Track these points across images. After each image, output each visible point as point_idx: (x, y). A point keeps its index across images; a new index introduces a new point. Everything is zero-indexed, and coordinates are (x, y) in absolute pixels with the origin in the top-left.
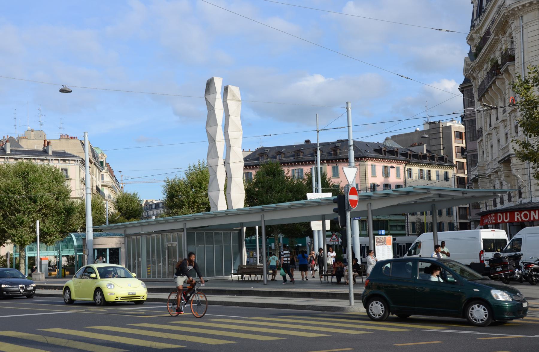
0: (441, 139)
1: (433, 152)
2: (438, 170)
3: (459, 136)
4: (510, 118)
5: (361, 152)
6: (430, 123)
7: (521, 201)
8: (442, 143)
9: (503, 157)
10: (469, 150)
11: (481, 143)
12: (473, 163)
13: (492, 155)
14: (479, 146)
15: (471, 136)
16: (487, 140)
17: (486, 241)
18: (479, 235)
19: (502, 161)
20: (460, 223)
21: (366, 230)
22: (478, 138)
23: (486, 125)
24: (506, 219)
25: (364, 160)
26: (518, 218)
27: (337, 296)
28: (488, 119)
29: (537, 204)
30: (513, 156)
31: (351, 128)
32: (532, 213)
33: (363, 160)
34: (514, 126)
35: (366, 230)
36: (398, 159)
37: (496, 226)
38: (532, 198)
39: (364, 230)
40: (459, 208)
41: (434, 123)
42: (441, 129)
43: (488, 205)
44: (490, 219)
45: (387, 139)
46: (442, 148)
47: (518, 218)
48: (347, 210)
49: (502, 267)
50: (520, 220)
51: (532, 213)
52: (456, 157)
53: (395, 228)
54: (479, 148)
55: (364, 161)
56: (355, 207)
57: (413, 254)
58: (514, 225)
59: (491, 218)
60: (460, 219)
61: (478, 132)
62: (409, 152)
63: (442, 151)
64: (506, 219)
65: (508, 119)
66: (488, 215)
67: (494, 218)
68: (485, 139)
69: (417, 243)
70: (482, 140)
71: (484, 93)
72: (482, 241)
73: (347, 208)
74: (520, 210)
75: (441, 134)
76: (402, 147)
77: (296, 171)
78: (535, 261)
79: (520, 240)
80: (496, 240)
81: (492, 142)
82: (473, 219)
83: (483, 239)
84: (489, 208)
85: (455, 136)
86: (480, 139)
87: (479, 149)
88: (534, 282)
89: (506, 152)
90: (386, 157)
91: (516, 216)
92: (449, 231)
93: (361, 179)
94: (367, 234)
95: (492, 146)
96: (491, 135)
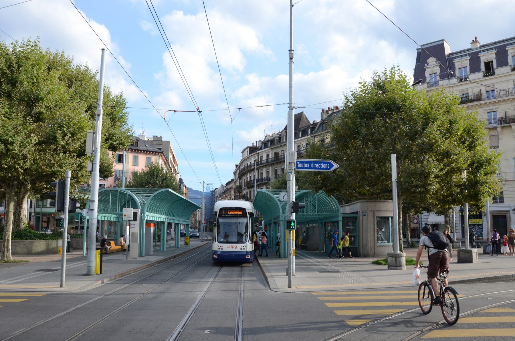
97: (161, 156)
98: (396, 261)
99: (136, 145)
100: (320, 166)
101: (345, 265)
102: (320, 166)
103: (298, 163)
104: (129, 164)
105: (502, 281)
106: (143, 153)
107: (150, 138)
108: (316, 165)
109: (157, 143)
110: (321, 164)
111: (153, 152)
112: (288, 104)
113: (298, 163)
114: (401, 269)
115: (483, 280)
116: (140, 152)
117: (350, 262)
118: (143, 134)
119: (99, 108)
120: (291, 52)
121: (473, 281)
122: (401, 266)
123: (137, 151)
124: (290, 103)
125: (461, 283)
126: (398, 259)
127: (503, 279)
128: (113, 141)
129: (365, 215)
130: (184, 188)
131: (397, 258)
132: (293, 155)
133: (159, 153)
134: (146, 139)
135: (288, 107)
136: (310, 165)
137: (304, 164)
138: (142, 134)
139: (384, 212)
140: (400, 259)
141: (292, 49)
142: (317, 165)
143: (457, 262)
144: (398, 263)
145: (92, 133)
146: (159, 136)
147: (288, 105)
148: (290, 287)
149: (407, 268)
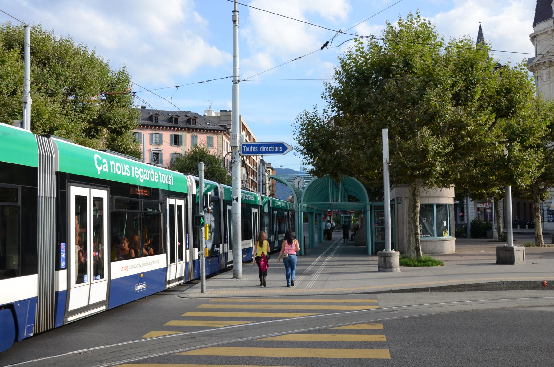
77: (154, 135)
97: (225, 134)
98: (385, 261)
99: (195, 123)
100: (271, 149)
101: (344, 265)
102: (271, 149)
103: (245, 146)
104: (186, 145)
105: (486, 290)
106: (202, 132)
107: (219, 113)
108: (266, 149)
109: (226, 118)
110: (272, 147)
111: (214, 130)
112: (232, 77)
113: (245, 146)
114: (391, 271)
115: (458, 288)
116: (206, 132)
117: (484, 256)
118: (210, 108)
119: (26, 94)
120: (235, 13)
121: (441, 289)
122: (391, 267)
123: (195, 130)
124: (234, 77)
125: (423, 290)
126: (387, 258)
127: (488, 287)
128: (112, 125)
129: (400, 203)
130: (271, 170)
131: (386, 258)
132: (234, 138)
133: (221, 131)
134: (214, 115)
135: (232, 81)
136: (259, 149)
137: (252, 148)
138: (208, 109)
139: (425, 198)
140: (390, 259)
141: (237, 10)
142: (267, 148)
143: (496, 262)
144: (387, 264)
145: (19, 124)
146: (228, 111)
147: (232, 79)
148: (202, 292)
149: (402, 271)
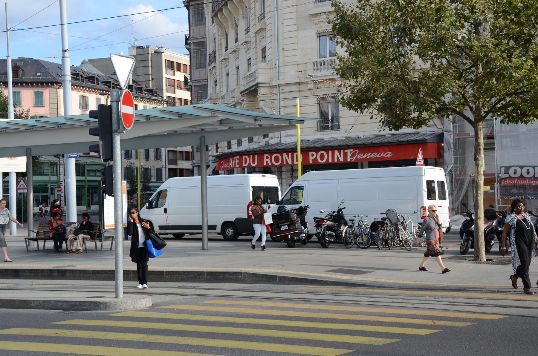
0: (150, 68)
1: (139, 83)
2: (145, 105)
3: (170, 67)
4: (256, 39)
5: (51, 76)
6: (138, 48)
7: (268, 141)
8: (150, 73)
9: (247, 87)
10: (195, 79)
11: (213, 70)
12: (199, 95)
13: (227, 86)
14: (210, 73)
15: (198, 63)
16: (222, 66)
17: (256, 190)
18: (247, 181)
19: (246, 92)
20: (169, 169)
21: (57, 175)
22: (210, 65)
23: (221, 47)
24: (254, 163)
25: (55, 86)
26: (267, 162)
27: (68, 274)
28: (224, 41)
29: (287, 145)
30: (261, 85)
31: (65, 27)
32: (285, 155)
33: (54, 86)
34: (260, 50)
35: (57, 175)
36: (99, 88)
37: (266, 170)
38: (282, 138)
39: (54, 175)
40: (169, 151)
41: (142, 47)
42: (150, 55)
43: (220, 147)
44: (233, 163)
45: (83, 63)
46: (151, 79)
47: (267, 162)
48: (116, 131)
49: (288, 225)
50: (270, 164)
51: (336, 152)
52: (167, 92)
53: (92, 174)
54: (210, 76)
55: (55, 88)
56: (129, 126)
57: (153, 206)
58: (256, 170)
59: (234, 162)
60: (169, 164)
61: (209, 57)
62: (112, 80)
63: (151, 82)
64: (254, 163)
65: (253, 40)
66: (230, 157)
67: (237, 161)
68: (219, 66)
69: (160, 191)
70: (214, 67)
71: (222, 6)
72: (252, 189)
73: (115, 127)
74: (271, 152)
75: (150, 62)
76: (103, 74)
78: (326, 217)
79: (300, 188)
80: (267, 187)
81: (228, 69)
82: (197, 164)
83: (252, 187)
84: (221, 150)
85: (166, 66)
86: (212, 65)
87: (210, 77)
88: (326, 244)
89: (252, 81)
90: (84, 84)
91: (266, 160)
92: (369, 168)
93: (51, 110)
94: (58, 180)
95: (228, 74)
96: (227, 61)
